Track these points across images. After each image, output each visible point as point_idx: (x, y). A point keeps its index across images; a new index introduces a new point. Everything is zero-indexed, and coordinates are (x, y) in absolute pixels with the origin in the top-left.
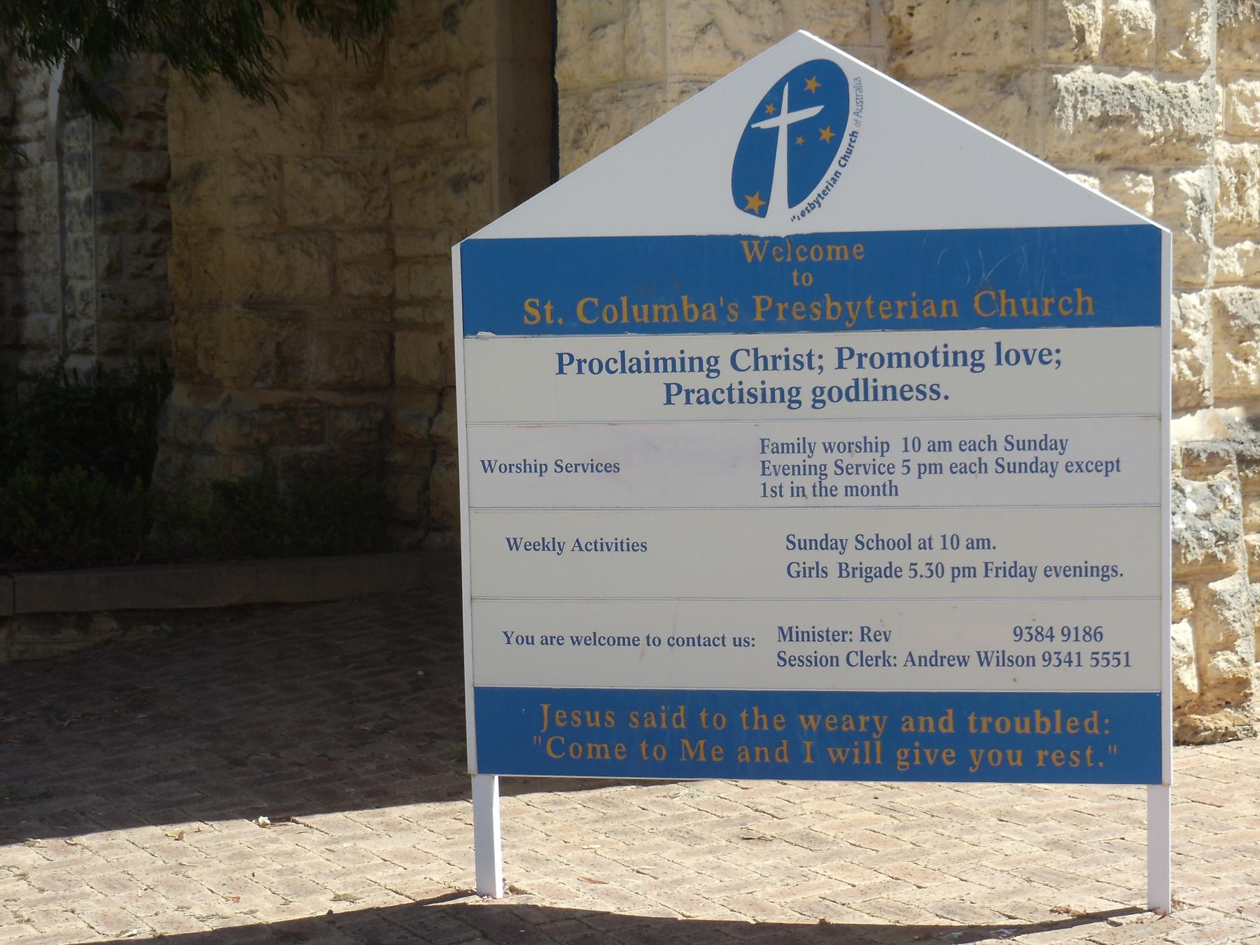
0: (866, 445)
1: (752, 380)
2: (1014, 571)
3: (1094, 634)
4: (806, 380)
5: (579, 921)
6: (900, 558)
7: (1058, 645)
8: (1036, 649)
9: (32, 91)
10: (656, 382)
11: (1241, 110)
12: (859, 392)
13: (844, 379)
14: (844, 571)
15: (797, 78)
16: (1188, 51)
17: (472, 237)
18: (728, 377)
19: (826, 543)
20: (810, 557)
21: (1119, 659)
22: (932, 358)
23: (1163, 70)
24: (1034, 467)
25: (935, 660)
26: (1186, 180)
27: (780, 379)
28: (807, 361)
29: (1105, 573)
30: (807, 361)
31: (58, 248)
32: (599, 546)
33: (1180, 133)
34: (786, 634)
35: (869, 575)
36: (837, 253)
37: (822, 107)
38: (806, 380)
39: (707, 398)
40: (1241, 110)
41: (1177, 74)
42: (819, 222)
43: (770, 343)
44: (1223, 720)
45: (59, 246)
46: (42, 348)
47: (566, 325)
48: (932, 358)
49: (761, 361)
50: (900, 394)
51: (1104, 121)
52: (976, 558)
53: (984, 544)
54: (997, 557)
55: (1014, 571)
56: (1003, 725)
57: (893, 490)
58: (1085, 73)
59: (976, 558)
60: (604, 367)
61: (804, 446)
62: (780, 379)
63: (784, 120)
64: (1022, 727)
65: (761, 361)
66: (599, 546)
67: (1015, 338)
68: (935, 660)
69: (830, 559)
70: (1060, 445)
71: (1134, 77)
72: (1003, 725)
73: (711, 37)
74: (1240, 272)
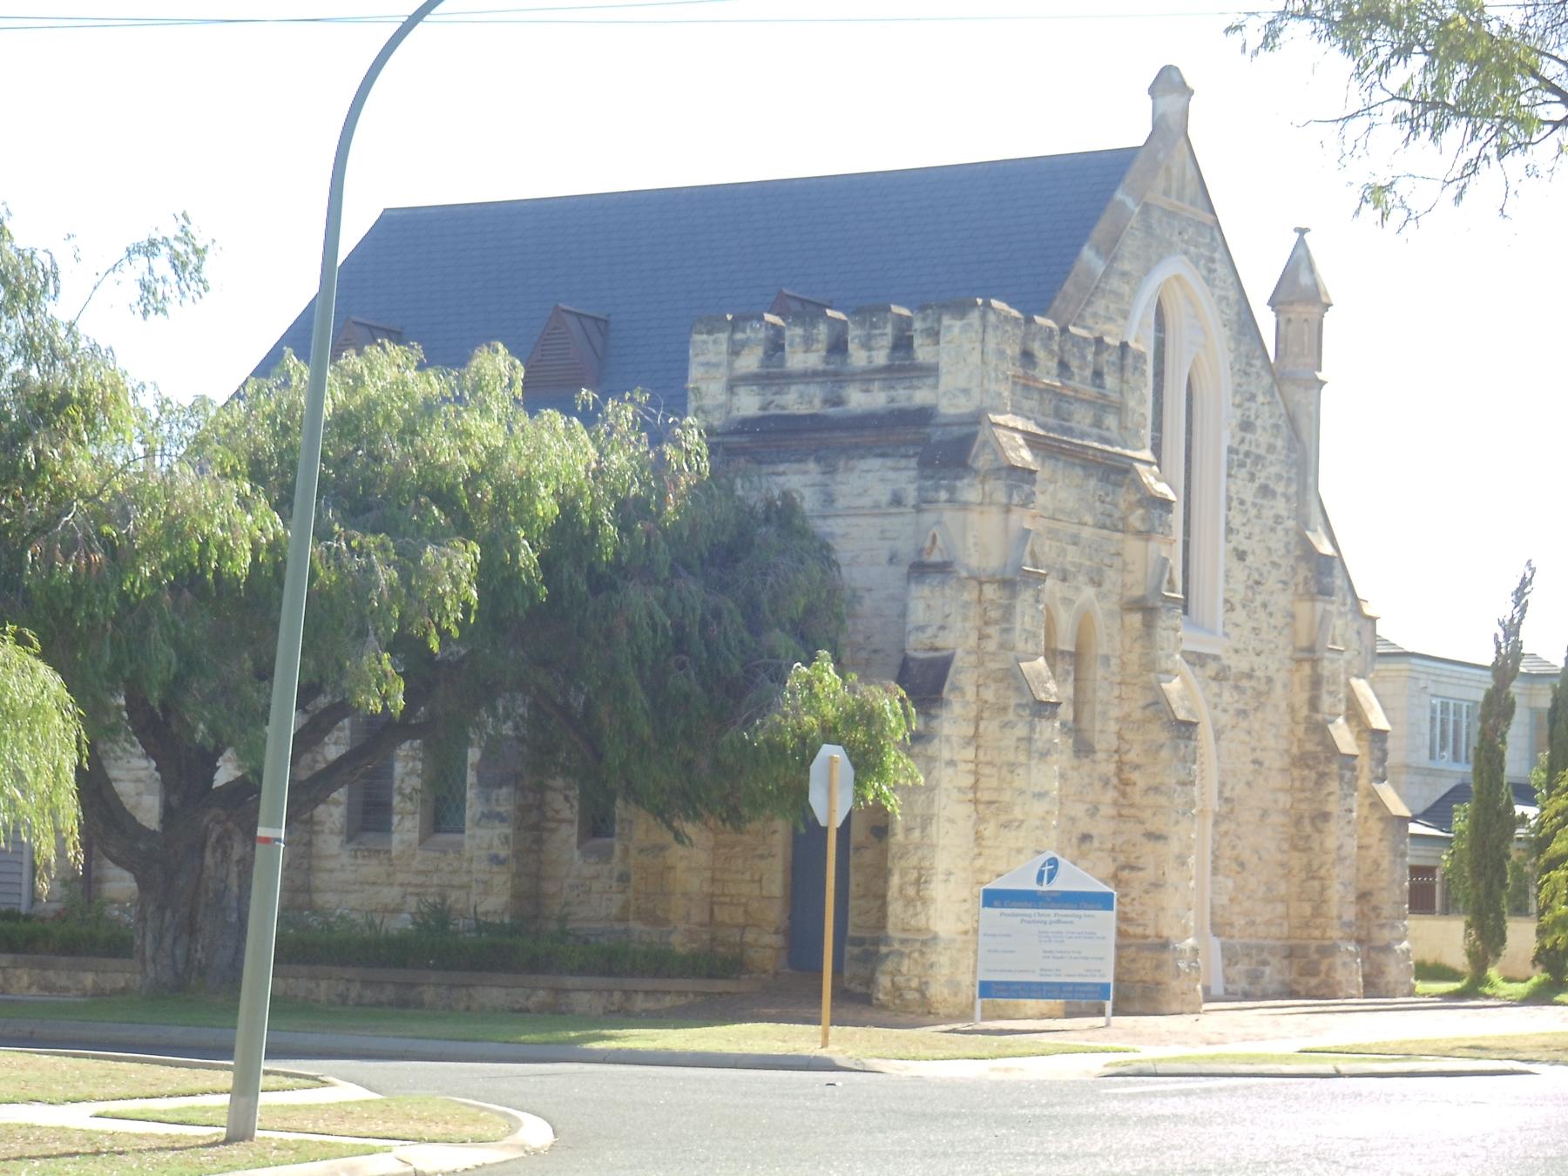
2: (1086, 958)
5: (40, 467)
9: (505, 882)
10: (1019, 918)
12: (1058, 922)
13: (1055, 919)
19: (1051, 952)
27: (1043, 918)
31: (70, 1159)
37: (216, 784)
38: (1048, 919)
43: (1041, 911)
45: (1043, 638)
46: (921, 629)
47: (1002, 906)
49: (1040, 915)
55: (1086, 958)
56: (1082, 989)
62: (1043, 918)
63: (1047, 868)
65: (1040, 915)
67: (1087, 912)
72: (1082, 989)
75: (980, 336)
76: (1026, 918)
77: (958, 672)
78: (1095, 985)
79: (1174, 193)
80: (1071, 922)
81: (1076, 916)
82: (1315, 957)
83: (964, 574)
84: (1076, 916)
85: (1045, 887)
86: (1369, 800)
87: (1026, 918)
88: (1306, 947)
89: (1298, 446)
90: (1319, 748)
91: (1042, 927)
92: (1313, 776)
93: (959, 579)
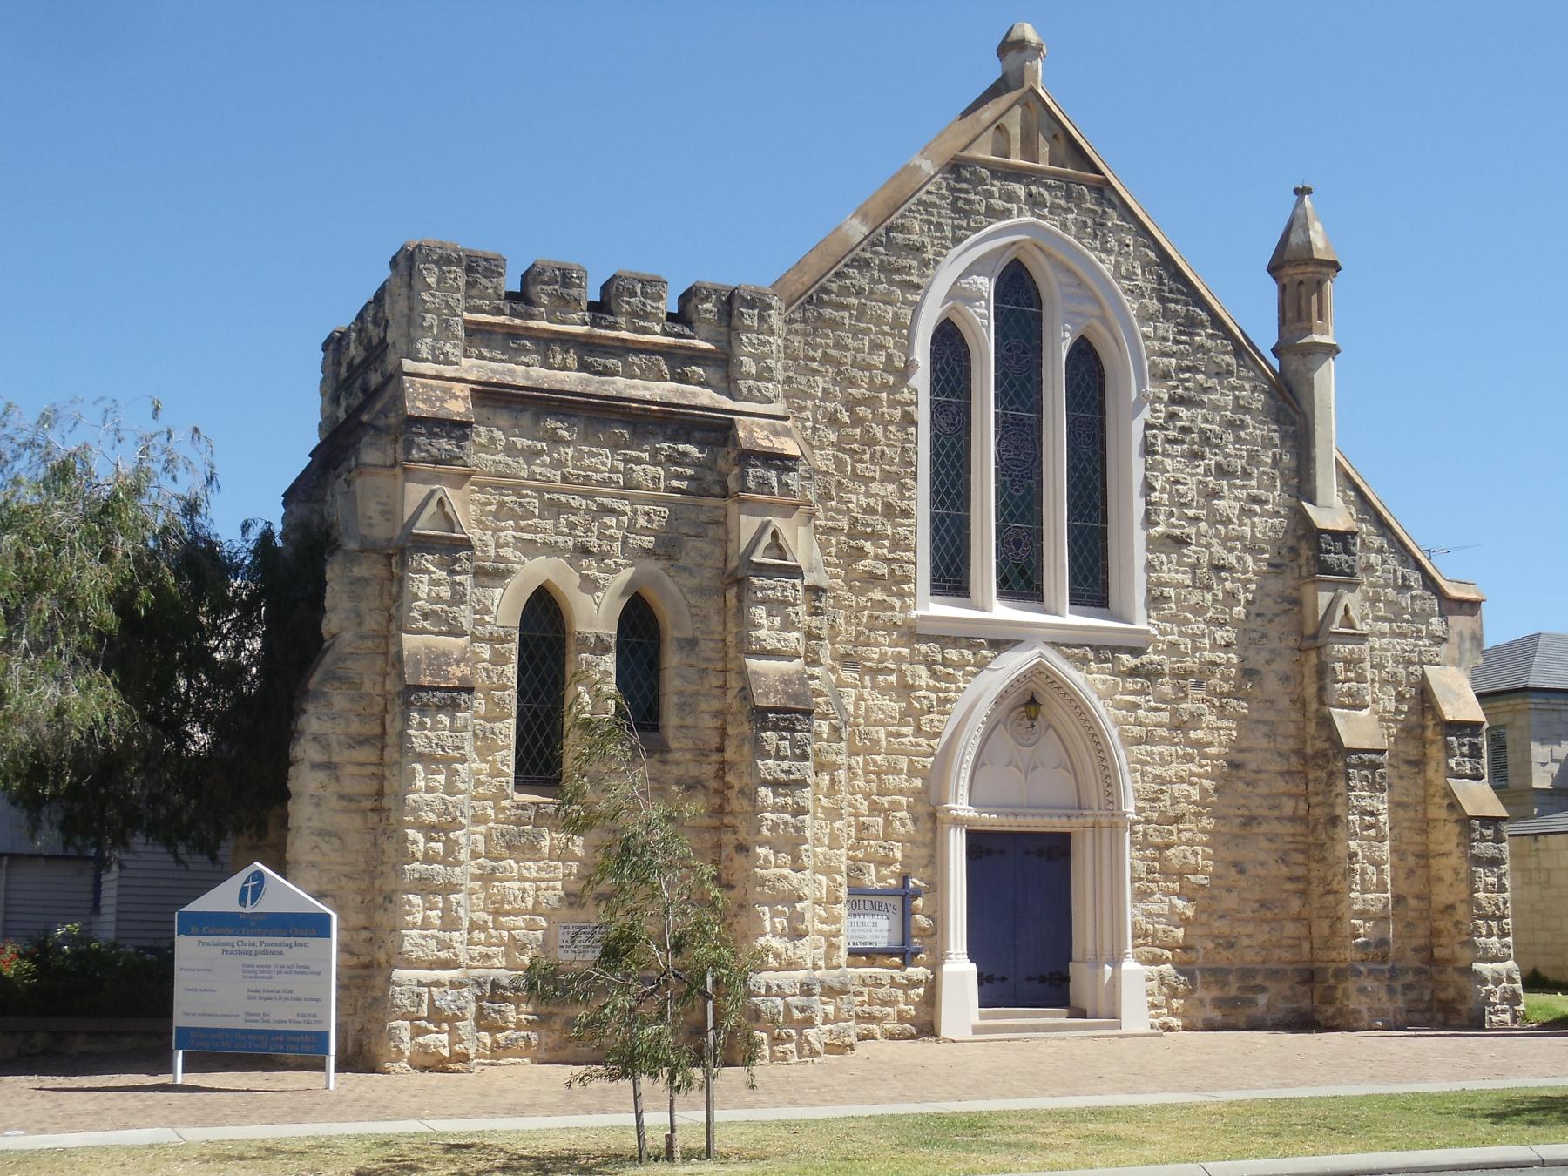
0: (266, 966)
1: (241, 949)
2: (298, 999)
3: (315, 1016)
4: (253, 949)
6: (273, 995)
7: (307, 1018)
8: (301, 1019)
10: (219, 948)
11: (524, 872)
12: (265, 952)
14: (260, 998)
15: (253, 874)
16: (455, 858)
17: (184, 909)
18: (236, 948)
19: (256, 991)
20: (253, 994)
21: (320, 1022)
22: (281, 944)
23: (446, 864)
24: (303, 973)
25: (280, 1021)
26: (453, 897)
27: (248, 948)
28: (254, 944)
29: (318, 1000)
30: (254, 944)
32: (205, 990)
33: (450, 883)
34: (247, 1014)
35: (266, 999)
36: (261, 917)
38: (253, 949)
39: (232, 953)
40: (524, 872)
41: (452, 865)
42: (257, 910)
43: (246, 939)
44: (458, 1066)
48: (281, 944)
50: (273, 953)
51: (420, 879)
52: (289, 996)
53: (291, 992)
54: (294, 995)
55: (298, 999)
57: (271, 977)
58: (416, 865)
59: (289, 996)
60: (208, 944)
61: (252, 966)
62: (248, 948)
64: (298, 1039)
65: (244, 944)
66: (205, 990)
68: (280, 1021)
69: (257, 995)
70: (308, 967)
71: (435, 866)
73: (316, 850)
74: (523, 925)
75: (406, 278)
76: (229, 948)
77: (342, 658)
78: (309, 1033)
79: (1016, 146)
80: (281, 953)
81: (287, 945)
82: (1332, 981)
83: (352, 545)
84: (287, 945)
85: (249, 909)
86: (1447, 801)
87: (229, 948)
88: (1325, 970)
89: (1297, 417)
90: (1327, 745)
91: (247, 960)
92: (1324, 775)
93: (346, 553)
